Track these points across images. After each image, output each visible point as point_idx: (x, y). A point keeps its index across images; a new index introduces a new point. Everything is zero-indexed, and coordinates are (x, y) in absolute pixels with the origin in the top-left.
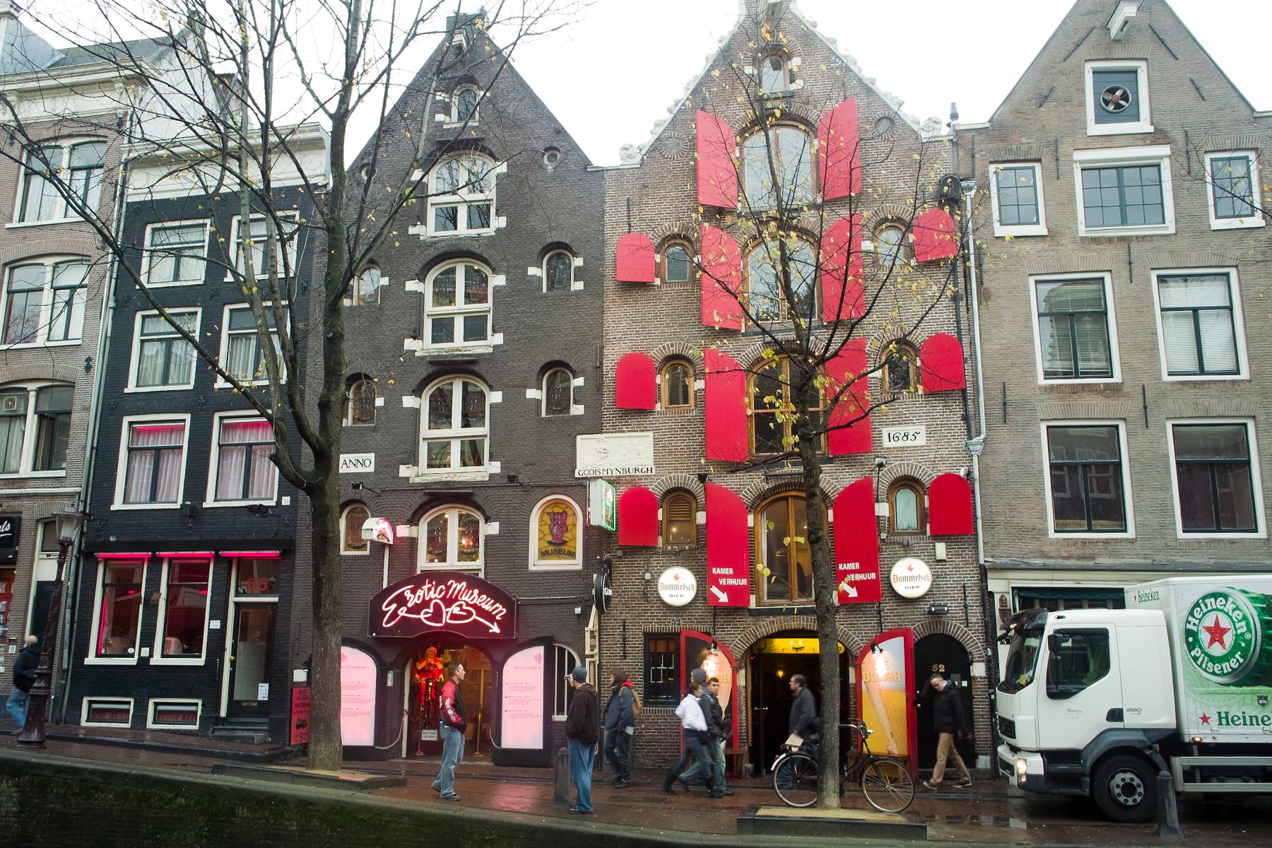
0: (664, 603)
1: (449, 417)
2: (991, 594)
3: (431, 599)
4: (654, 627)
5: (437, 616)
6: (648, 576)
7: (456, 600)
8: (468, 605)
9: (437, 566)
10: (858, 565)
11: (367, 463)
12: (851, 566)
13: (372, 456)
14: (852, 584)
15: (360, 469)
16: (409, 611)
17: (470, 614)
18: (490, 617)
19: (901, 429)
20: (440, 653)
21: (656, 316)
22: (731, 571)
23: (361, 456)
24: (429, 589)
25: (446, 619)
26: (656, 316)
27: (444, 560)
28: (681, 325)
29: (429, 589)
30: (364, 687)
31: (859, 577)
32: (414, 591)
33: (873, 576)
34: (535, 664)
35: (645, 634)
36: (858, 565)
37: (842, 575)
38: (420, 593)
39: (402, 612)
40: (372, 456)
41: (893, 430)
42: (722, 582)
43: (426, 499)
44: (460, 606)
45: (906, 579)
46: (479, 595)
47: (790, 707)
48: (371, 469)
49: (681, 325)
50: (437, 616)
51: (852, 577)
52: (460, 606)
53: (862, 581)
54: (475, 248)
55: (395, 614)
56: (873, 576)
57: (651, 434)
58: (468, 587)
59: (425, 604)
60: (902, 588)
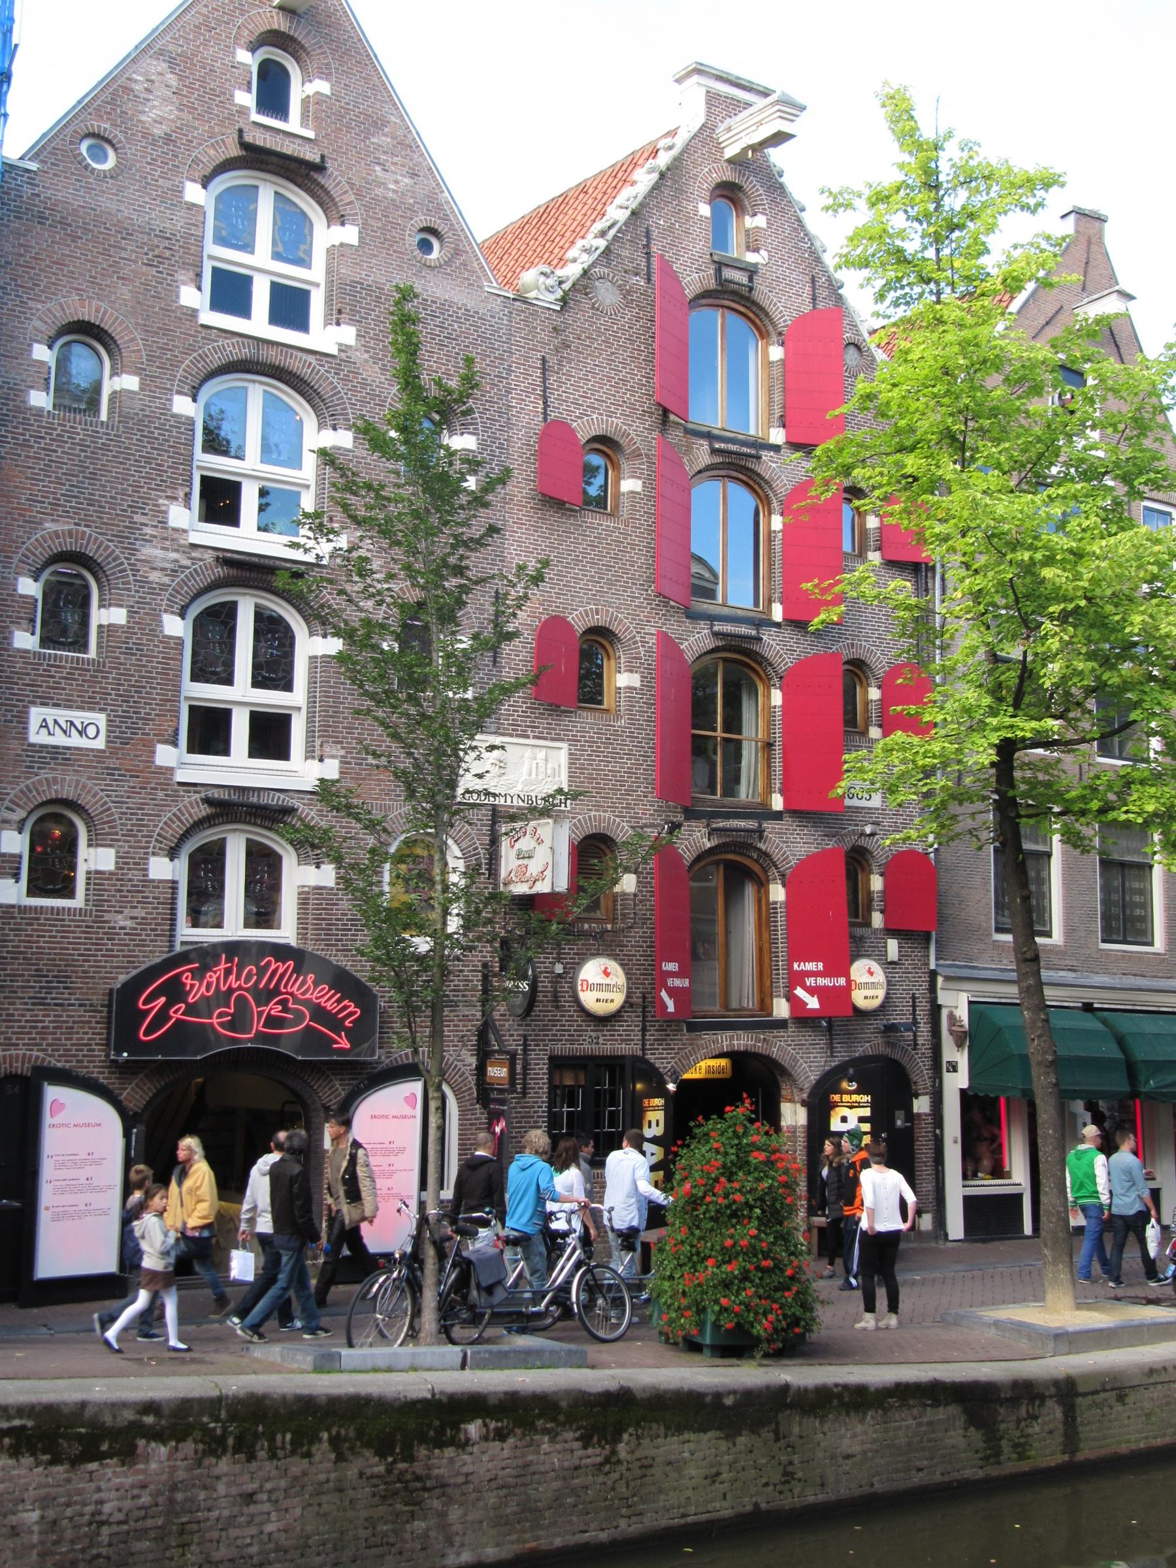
0: (582, 1009)
2: (939, 1007)
4: (563, 1048)
5: (238, 1022)
6: (559, 969)
7: (276, 992)
8: (297, 1001)
9: (207, 935)
10: (821, 966)
11: (91, 731)
12: (810, 966)
13: (101, 719)
14: (811, 991)
15: (75, 741)
17: (300, 1016)
18: (334, 1022)
20: (1108, 1147)
23: (79, 717)
24: (228, 972)
25: (258, 1026)
28: (610, 583)
29: (228, 972)
30: (98, 1162)
31: (822, 981)
33: (842, 981)
34: (407, 1110)
35: (552, 1059)
36: (821, 966)
37: (797, 979)
39: (177, 1013)
40: (101, 719)
42: (810, 981)
44: (283, 1003)
45: (600, 987)
46: (316, 984)
48: (100, 744)
49: (610, 583)
50: (238, 1022)
51: (810, 981)
52: (283, 1003)
53: (826, 988)
55: (163, 1016)
56: (842, 981)
57: (565, 745)
58: (298, 970)
60: (589, 999)
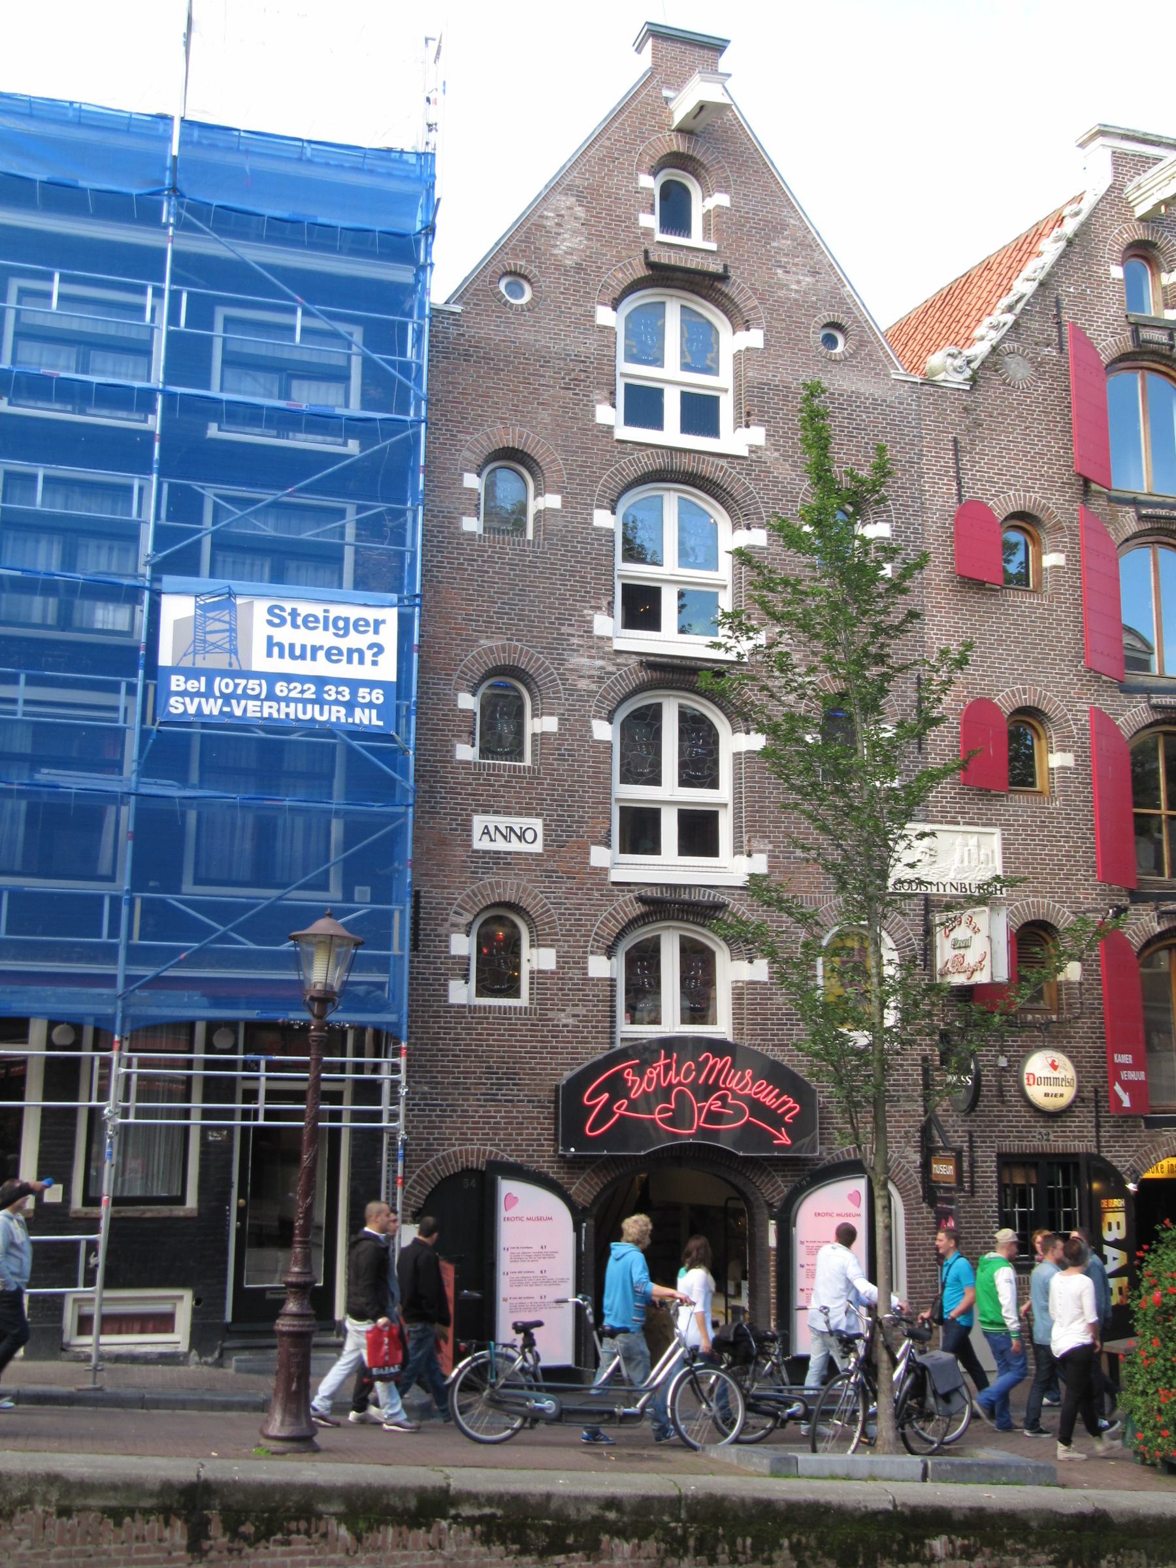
0: (1030, 1104)
1: (657, 765)
3: (671, 1086)
4: (1013, 1145)
6: (1003, 1062)
7: (715, 1087)
8: (736, 1096)
9: (646, 1032)
11: (529, 836)
13: (537, 824)
16: (633, 1106)
17: (739, 1113)
19: (503, 821)
21: (1000, 641)
22: (49, 1180)
23: (518, 822)
24: (667, 1068)
26: (1000, 641)
27: (656, 1021)
28: (1036, 661)
29: (667, 1068)
32: (640, 1071)
35: (1000, 1156)
38: (652, 1073)
39: (621, 1108)
40: (537, 824)
41: (491, 820)
42: (1124, 1075)
43: (639, 909)
44: (723, 1098)
47: (1172, 1278)
48: (538, 847)
49: (1036, 661)
52: (723, 1098)
54: (707, 469)
55: (607, 1112)
59: (665, 1093)
